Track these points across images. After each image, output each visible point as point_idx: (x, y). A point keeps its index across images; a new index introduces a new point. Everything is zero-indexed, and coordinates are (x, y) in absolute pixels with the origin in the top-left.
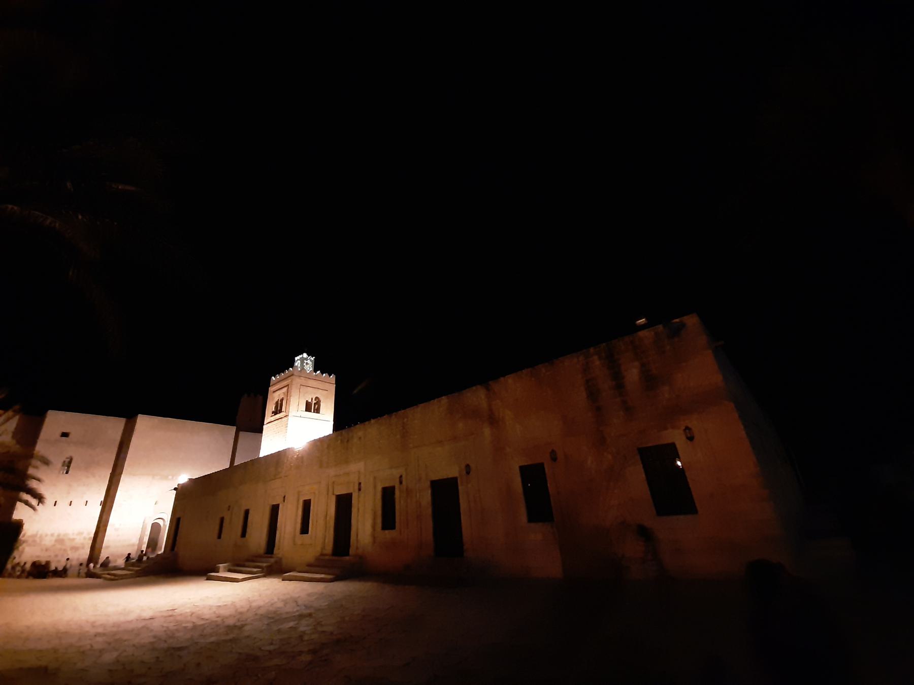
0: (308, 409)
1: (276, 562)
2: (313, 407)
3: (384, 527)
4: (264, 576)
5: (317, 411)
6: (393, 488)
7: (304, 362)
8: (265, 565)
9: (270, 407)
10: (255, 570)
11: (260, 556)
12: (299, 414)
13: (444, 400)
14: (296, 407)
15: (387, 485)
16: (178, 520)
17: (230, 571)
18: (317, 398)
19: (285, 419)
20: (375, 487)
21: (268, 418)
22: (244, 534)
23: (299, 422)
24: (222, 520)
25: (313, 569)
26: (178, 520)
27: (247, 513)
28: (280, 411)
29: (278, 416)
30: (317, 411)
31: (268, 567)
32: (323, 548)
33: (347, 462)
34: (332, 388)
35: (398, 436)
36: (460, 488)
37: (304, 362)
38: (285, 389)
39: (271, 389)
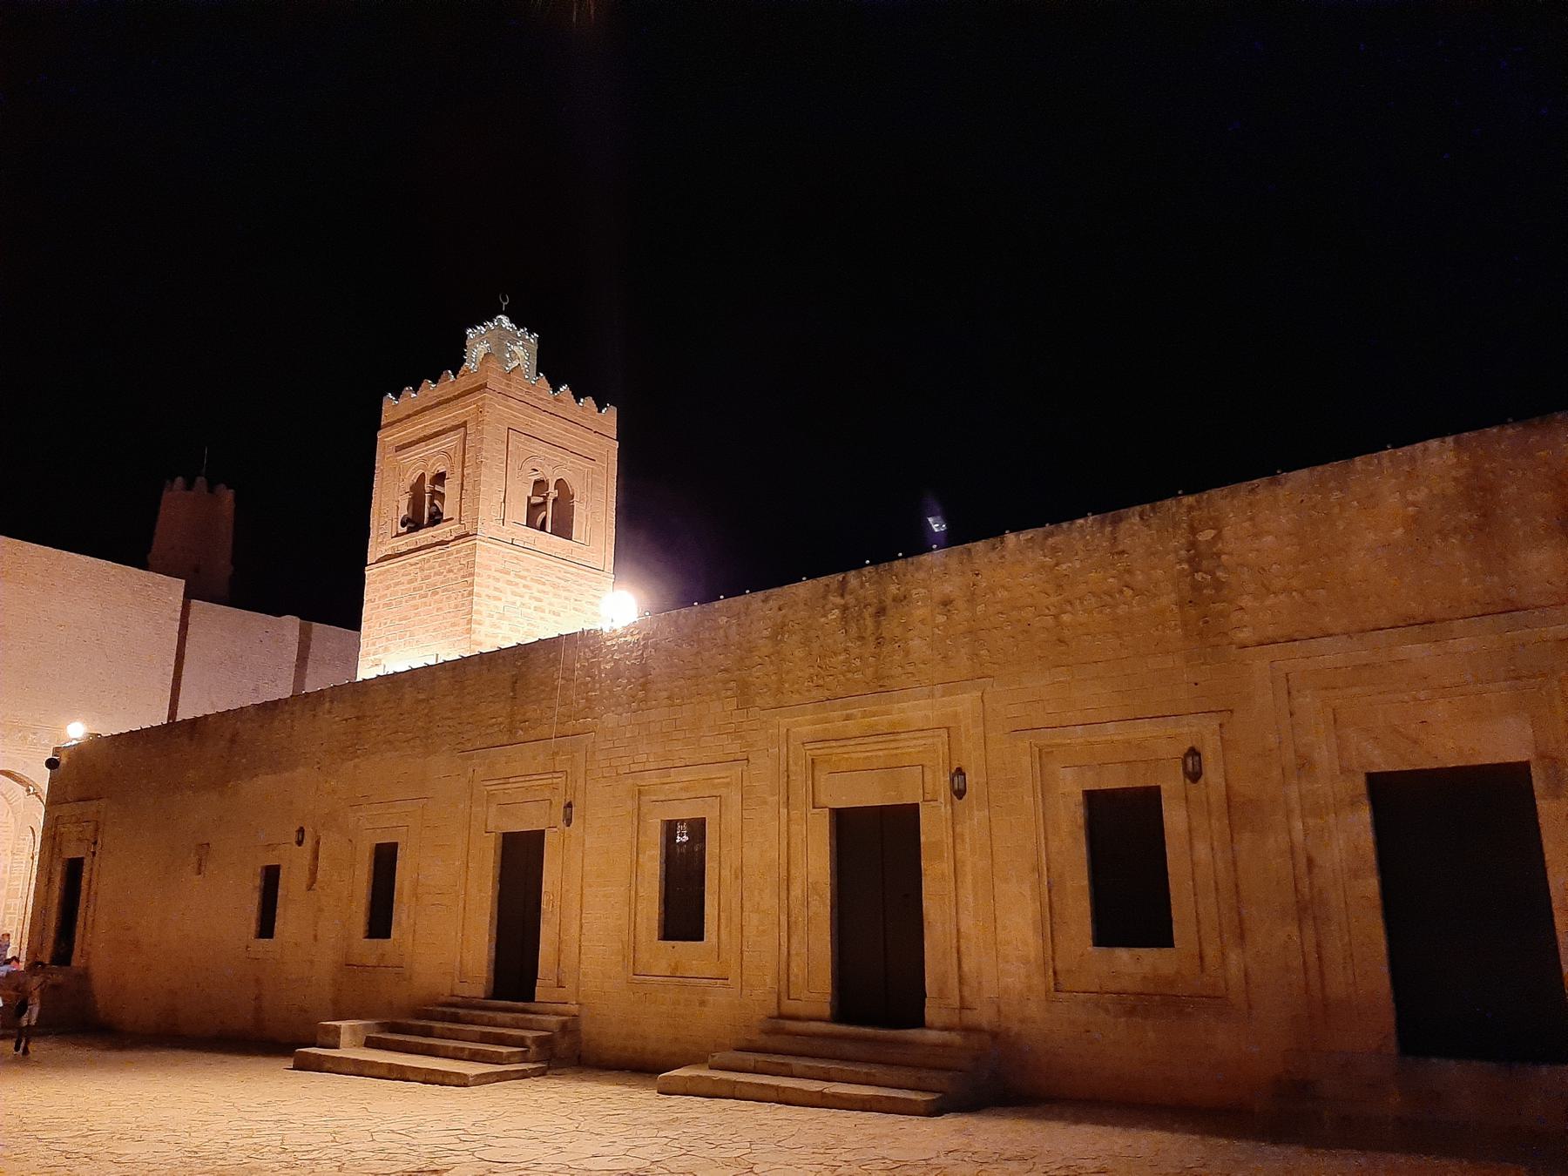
0: (533, 518)
1: (564, 1027)
2: (551, 512)
3: (1108, 932)
4: (541, 1073)
5: (563, 529)
6: (1149, 799)
7: (501, 348)
8: (530, 1034)
9: (388, 503)
10: (504, 1050)
11: (468, 1004)
12: (508, 531)
13: (1440, 457)
14: (495, 507)
15: (1114, 780)
16: (74, 869)
17: (371, 1043)
18: (560, 484)
19: (462, 545)
20: (1045, 788)
21: (384, 535)
22: (380, 922)
23: (509, 552)
24: (271, 876)
25: (751, 1058)
26: (74, 869)
27: (385, 859)
28: (436, 518)
29: (425, 536)
30: (563, 529)
31: (539, 1041)
32: (785, 988)
33: (881, 686)
34: (610, 449)
35: (1168, 599)
36: (1543, 805)
37: (501, 348)
38: (451, 441)
39: (386, 439)
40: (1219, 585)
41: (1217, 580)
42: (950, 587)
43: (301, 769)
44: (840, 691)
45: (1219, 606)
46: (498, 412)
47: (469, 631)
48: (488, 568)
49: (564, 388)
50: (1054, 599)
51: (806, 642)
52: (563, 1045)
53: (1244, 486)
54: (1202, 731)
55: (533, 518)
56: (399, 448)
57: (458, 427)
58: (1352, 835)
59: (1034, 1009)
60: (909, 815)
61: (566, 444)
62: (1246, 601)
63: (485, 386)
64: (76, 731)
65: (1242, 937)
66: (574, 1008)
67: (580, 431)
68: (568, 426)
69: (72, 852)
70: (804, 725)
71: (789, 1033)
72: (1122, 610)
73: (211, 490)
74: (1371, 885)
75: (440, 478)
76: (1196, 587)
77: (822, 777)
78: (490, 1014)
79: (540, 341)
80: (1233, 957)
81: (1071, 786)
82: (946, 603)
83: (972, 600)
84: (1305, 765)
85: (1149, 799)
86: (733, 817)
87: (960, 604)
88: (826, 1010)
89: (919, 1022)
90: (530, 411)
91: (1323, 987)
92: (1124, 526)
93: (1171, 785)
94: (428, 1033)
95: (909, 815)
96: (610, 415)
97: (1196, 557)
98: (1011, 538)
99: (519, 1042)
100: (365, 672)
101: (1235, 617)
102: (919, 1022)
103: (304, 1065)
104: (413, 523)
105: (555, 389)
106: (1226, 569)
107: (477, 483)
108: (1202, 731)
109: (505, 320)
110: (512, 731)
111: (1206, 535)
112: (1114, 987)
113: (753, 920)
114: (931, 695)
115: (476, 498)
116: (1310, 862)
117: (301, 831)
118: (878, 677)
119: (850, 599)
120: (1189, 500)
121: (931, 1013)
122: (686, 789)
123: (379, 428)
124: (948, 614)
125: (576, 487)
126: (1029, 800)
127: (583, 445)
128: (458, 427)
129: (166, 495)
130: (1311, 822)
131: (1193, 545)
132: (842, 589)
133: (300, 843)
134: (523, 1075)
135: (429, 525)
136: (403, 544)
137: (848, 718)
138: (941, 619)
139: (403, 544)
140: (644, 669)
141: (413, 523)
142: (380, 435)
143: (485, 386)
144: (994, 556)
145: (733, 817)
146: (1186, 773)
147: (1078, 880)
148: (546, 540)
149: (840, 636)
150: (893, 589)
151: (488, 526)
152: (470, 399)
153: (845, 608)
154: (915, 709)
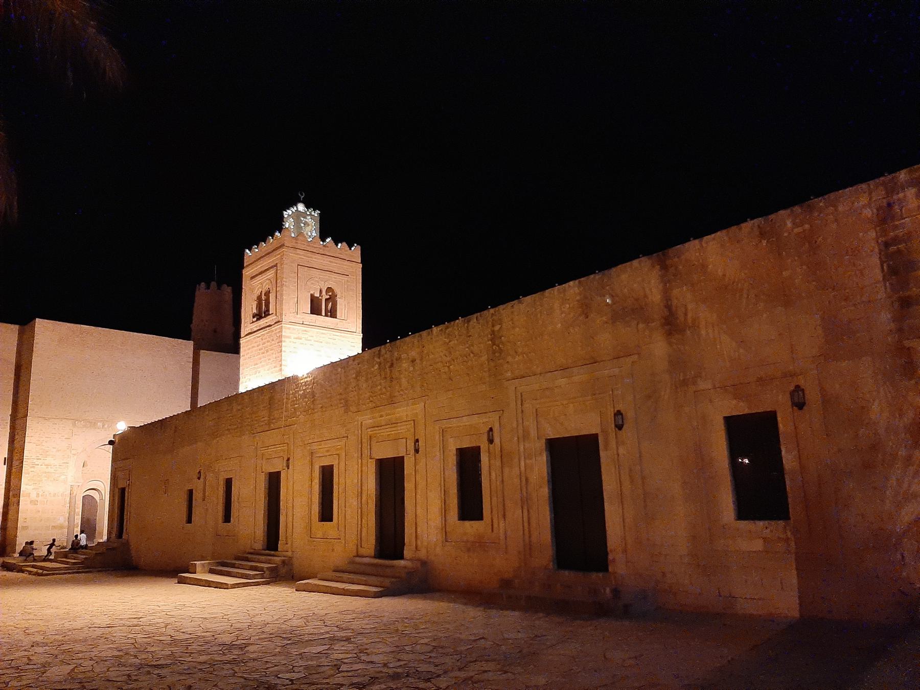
0: (315, 309)
4: (267, 583)
5: (332, 313)
7: (302, 221)
9: (248, 307)
12: (300, 318)
13: (572, 288)
14: (293, 306)
16: (123, 490)
17: (212, 571)
19: (277, 327)
20: (444, 449)
21: (247, 326)
23: (303, 328)
24: (191, 492)
27: (229, 483)
28: (267, 313)
29: (263, 322)
30: (332, 313)
31: (271, 570)
33: (392, 401)
34: (356, 270)
35: (484, 358)
37: (302, 221)
39: (247, 273)
40: (501, 351)
41: (500, 349)
42: (414, 354)
43: (199, 444)
44: (378, 404)
45: (501, 361)
46: (291, 258)
47: (281, 370)
48: (289, 337)
49: (328, 240)
50: (448, 359)
51: (367, 381)
52: (283, 571)
53: (510, 304)
54: (492, 419)
55: (315, 309)
56: (252, 278)
57: (272, 267)
58: (540, 467)
59: (438, 550)
60: (770, 418)
61: (331, 269)
62: (509, 359)
63: (283, 245)
64: (122, 427)
65: (504, 516)
66: (289, 554)
67: (339, 261)
68: (332, 259)
69: (121, 486)
70: (367, 419)
71: (359, 563)
72: (469, 364)
73: (219, 287)
74: (545, 491)
75: (267, 294)
76: (494, 352)
77: (373, 443)
78: (257, 557)
79: (320, 215)
80: (502, 524)
81: (453, 446)
82: (413, 361)
83: (421, 359)
84: (526, 436)
85: (476, 451)
86: (342, 464)
87: (418, 361)
88: (373, 554)
89: (401, 557)
90: (309, 254)
91: (530, 537)
92: (471, 323)
93: (484, 445)
94: (233, 566)
95: (770, 418)
96: (356, 250)
97: (495, 338)
98: (435, 329)
99: (261, 569)
100: (242, 389)
101: (506, 366)
102: (401, 557)
103: (182, 581)
104: (259, 316)
105: (324, 240)
106: (503, 343)
107: (282, 295)
108: (492, 419)
109: (301, 207)
110: (269, 424)
111: (497, 328)
112: (465, 539)
113: (349, 512)
114: (408, 405)
115: (281, 304)
116: (527, 480)
117: (200, 472)
118: (392, 397)
119: (382, 358)
120: (492, 311)
121: (407, 553)
122: (328, 451)
123: (243, 268)
124: (413, 366)
125: (337, 290)
126: (438, 454)
127: (343, 270)
128: (272, 267)
129: (197, 293)
130: (527, 461)
131: (493, 331)
132: (379, 355)
133: (199, 478)
134: (258, 584)
135: (265, 317)
136: (255, 326)
137: (381, 416)
138: (411, 369)
139: (255, 326)
140: (313, 395)
141: (259, 315)
142: (244, 272)
143: (283, 245)
144: (429, 337)
145: (342, 464)
146: (616, 426)
147: (454, 491)
148: (321, 320)
149: (378, 377)
150: (396, 354)
151: (288, 314)
152: (278, 252)
153: (380, 364)
154: (403, 411)
